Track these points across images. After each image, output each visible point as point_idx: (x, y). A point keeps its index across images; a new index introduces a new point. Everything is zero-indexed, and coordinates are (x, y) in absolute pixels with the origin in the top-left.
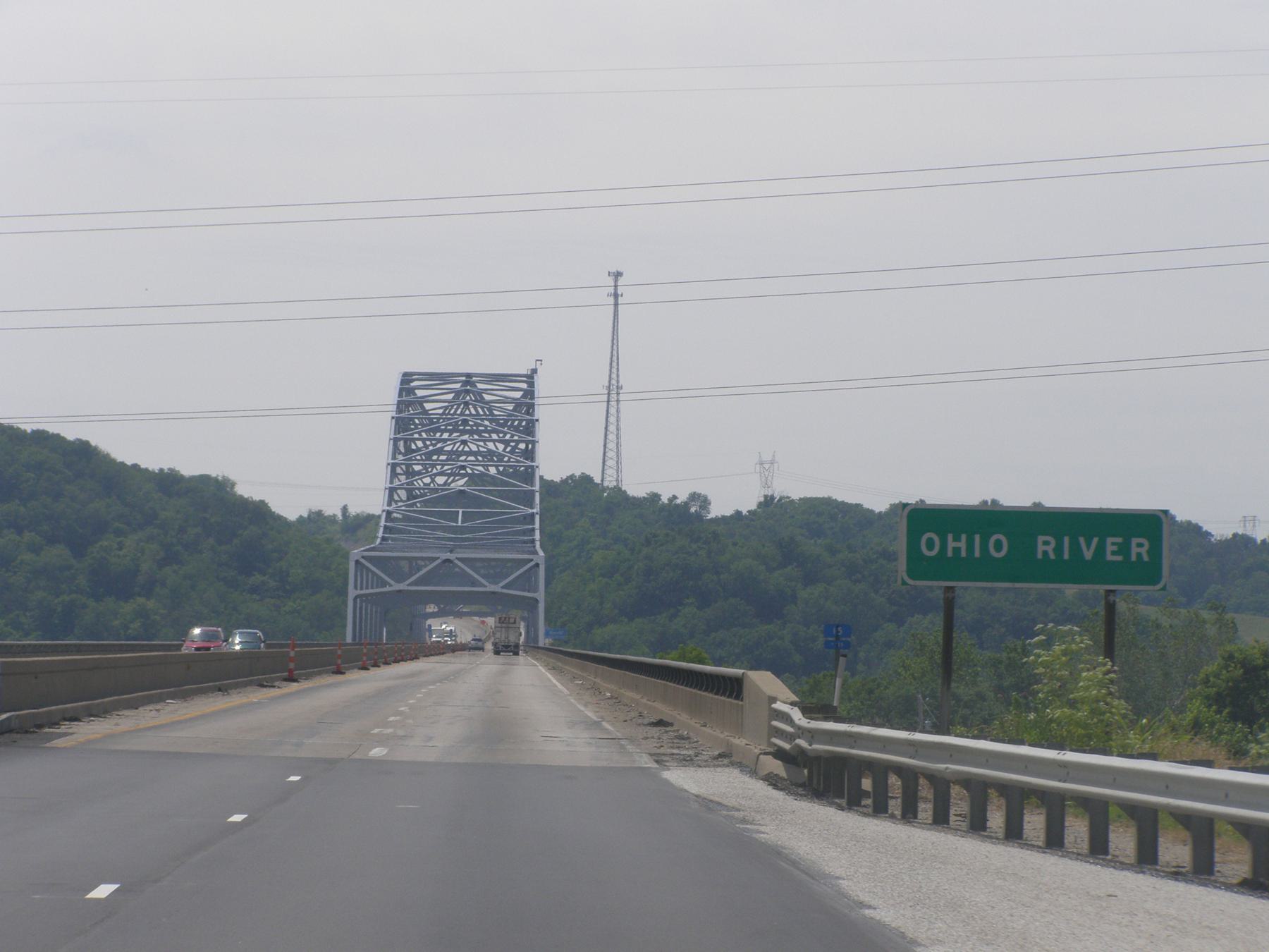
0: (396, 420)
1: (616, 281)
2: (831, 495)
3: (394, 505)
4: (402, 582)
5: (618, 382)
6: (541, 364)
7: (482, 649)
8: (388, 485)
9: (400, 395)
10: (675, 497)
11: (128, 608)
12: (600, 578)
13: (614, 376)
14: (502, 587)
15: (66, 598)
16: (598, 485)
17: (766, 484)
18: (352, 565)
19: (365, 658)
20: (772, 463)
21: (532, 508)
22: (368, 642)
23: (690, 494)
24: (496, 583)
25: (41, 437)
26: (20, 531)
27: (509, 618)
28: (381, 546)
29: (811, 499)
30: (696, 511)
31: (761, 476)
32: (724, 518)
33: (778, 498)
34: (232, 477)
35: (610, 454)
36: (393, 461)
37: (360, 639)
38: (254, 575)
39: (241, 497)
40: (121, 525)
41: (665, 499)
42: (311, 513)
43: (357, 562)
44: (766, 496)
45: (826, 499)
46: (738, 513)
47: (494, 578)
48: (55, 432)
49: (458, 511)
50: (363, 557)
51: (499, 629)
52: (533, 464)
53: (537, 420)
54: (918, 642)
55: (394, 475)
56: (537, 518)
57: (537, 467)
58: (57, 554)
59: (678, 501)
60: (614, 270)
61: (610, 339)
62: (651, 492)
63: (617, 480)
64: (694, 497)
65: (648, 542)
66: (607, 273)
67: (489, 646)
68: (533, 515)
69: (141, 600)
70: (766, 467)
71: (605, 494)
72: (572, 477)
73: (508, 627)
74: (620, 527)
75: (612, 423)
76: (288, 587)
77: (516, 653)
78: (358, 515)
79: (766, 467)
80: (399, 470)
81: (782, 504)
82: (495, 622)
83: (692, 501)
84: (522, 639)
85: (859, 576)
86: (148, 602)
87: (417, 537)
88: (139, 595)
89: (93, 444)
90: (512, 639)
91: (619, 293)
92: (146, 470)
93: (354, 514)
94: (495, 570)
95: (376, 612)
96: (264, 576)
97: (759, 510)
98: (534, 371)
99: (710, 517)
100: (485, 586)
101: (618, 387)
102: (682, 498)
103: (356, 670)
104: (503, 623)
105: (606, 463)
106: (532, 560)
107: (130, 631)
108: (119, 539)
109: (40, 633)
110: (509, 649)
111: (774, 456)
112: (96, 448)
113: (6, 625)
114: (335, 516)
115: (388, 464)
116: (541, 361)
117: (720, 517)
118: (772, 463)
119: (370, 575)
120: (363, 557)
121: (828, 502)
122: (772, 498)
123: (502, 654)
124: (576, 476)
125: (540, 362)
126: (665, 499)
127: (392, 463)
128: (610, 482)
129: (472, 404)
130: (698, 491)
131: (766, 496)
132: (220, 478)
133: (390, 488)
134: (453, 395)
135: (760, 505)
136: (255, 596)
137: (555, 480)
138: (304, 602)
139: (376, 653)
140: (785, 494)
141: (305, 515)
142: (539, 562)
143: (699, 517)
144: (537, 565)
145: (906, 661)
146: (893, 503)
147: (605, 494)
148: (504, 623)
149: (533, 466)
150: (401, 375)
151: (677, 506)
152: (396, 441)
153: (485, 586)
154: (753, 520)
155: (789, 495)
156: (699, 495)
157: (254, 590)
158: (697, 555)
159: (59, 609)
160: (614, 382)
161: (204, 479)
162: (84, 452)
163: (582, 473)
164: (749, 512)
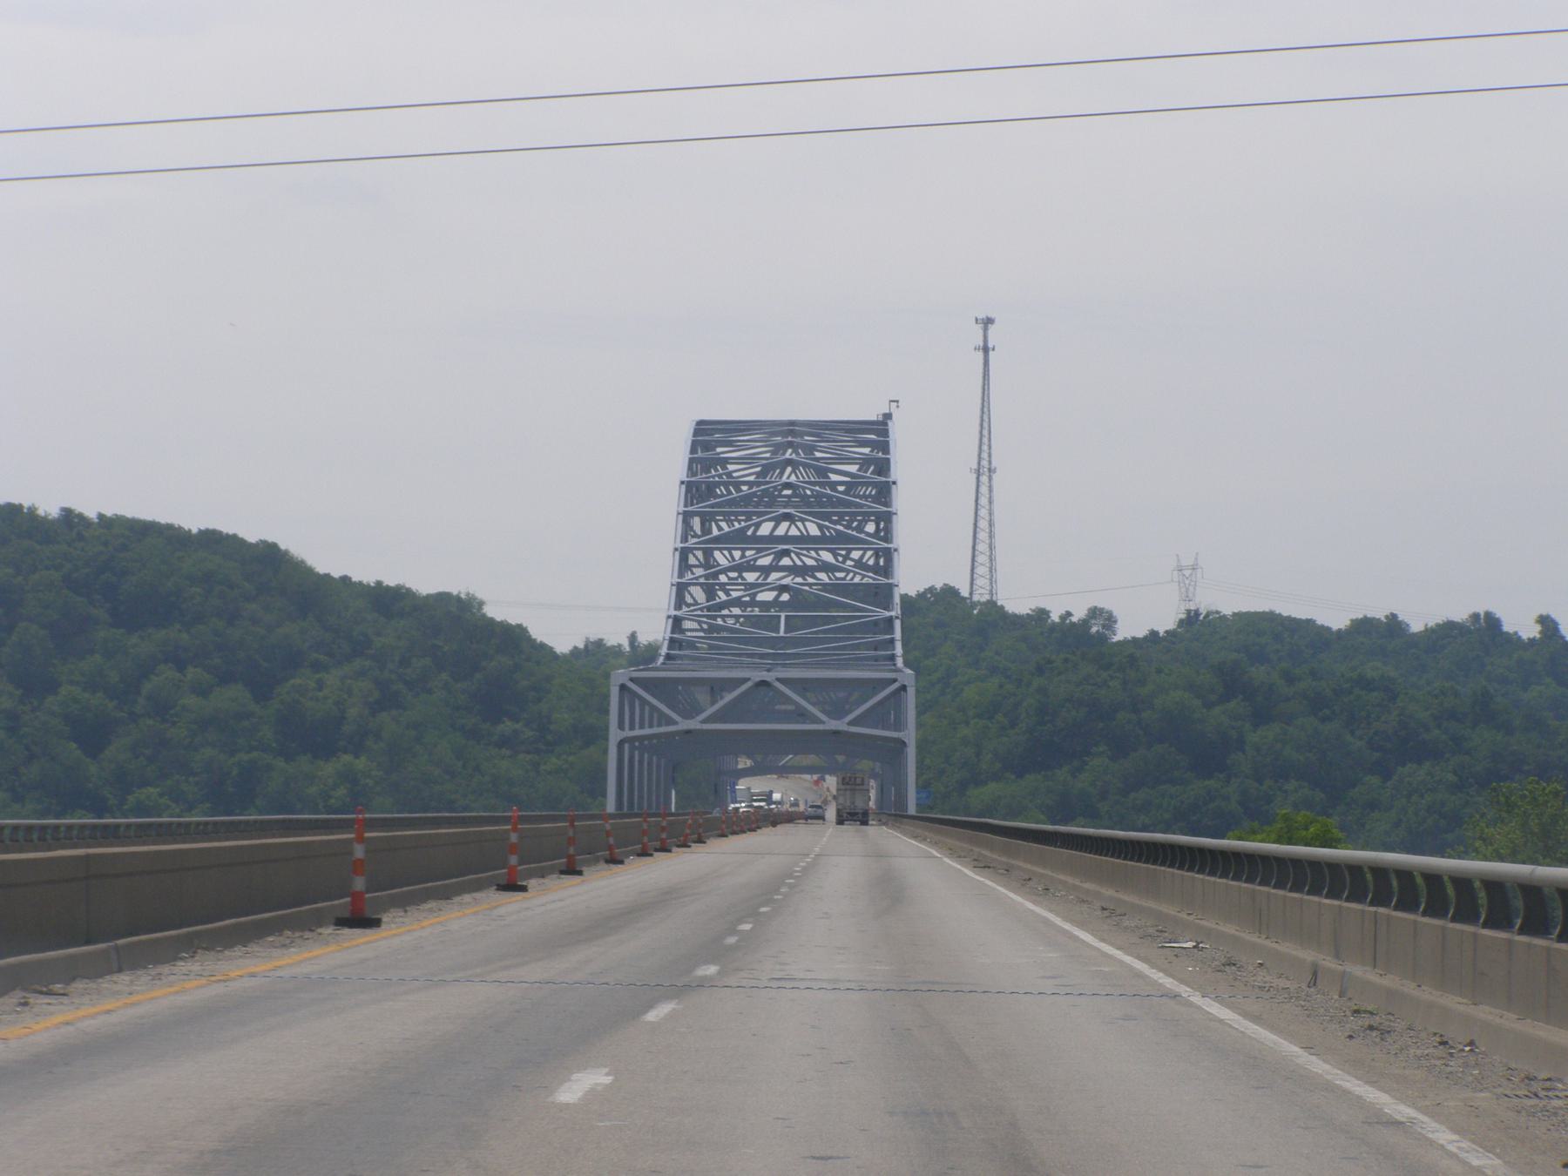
0: (687, 487)
1: (985, 330)
2: (1273, 608)
3: (685, 609)
4: (693, 718)
5: (990, 462)
6: (898, 407)
7: (822, 818)
8: (677, 580)
9: (693, 450)
10: (1069, 614)
11: (328, 769)
12: (976, 720)
13: (985, 455)
14: (851, 723)
15: (245, 757)
16: (964, 599)
17: (1187, 597)
18: (615, 693)
19: (359, 884)
20: (1194, 568)
21: (887, 608)
22: (653, 811)
23: (1090, 610)
24: (839, 718)
25: (212, 540)
26: (181, 666)
27: (855, 778)
28: (664, 666)
29: (1248, 614)
30: (1098, 631)
31: (1179, 585)
32: (1135, 641)
33: (1204, 613)
34: (480, 595)
35: (981, 559)
36: (682, 545)
37: (650, 806)
38: (504, 722)
39: (492, 620)
40: (322, 657)
41: (1055, 617)
42: (588, 643)
43: (623, 687)
44: (1189, 611)
45: (1267, 613)
46: (1154, 634)
47: (837, 712)
48: (231, 533)
49: (780, 616)
50: (632, 680)
51: (842, 792)
52: (890, 546)
53: (894, 483)
54: (1502, 799)
55: (684, 566)
56: (898, 624)
57: (896, 550)
58: (233, 697)
59: (1074, 619)
60: (982, 316)
61: (979, 406)
62: (1037, 608)
63: (991, 593)
64: (1095, 612)
65: (1040, 670)
66: (974, 319)
67: (831, 813)
68: (890, 620)
69: (347, 758)
70: (1187, 573)
71: (975, 612)
72: (931, 589)
73: (854, 790)
74: (997, 653)
75: (983, 507)
76: (549, 737)
77: (865, 823)
78: (650, 644)
79: (1187, 573)
80: (692, 561)
81: (1209, 622)
82: (838, 783)
83: (1092, 618)
84: (872, 804)
85: (1327, 711)
86: (357, 761)
87: (717, 654)
88: (345, 752)
89: (283, 547)
90: (860, 804)
91: (990, 345)
92: (360, 583)
93: (645, 643)
94: (836, 696)
95: (658, 766)
96: (517, 722)
97: (1179, 630)
98: (888, 416)
99: (1116, 639)
100: (823, 722)
101: (990, 470)
102: (1079, 614)
103: (328, 931)
104: (848, 784)
105: (975, 571)
106: (895, 680)
107: (333, 801)
108: (318, 676)
109: (208, 805)
110: (855, 818)
111: (1196, 559)
112: (286, 553)
113: (161, 795)
114: (620, 646)
115: (676, 549)
116: (897, 401)
117: (1130, 638)
118: (1194, 568)
119: (647, 708)
120: (632, 680)
121: (1271, 617)
122: (1197, 613)
123: (846, 822)
124: (936, 589)
125: (896, 404)
126: (1055, 617)
127: (682, 548)
128: (981, 596)
129: (795, 552)
130: (1100, 605)
131: (1189, 611)
132: (463, 596)
133: (678, 583)
134: (771, 557)
135: (1181, 622)
136: (504, 751)
137: (910, 594)
138: (571, 758)
139: (571, 841)
140: (1214, 608)
141: (581, 646)
142: (906, 683)
143: (1102, 639)
144: (904, 688)
145: (1486, 830)
146: (1354, 618)
147: (975, 612)
148: (851, 784)
149: (890, 548)
150: (694, 423)
151: (1073, 624)
152: (687, 517)
153: (823, 722)
154: (1174, 643)
155: (1219, 609)
156: (1101, 610)
157: (504, 742)
158: (1109, 687)
159: (235, 772)
160: (985, 463)
161: (443, 598)
162: (270, 558)
163: (945, 585)
164: (1166, 632)
